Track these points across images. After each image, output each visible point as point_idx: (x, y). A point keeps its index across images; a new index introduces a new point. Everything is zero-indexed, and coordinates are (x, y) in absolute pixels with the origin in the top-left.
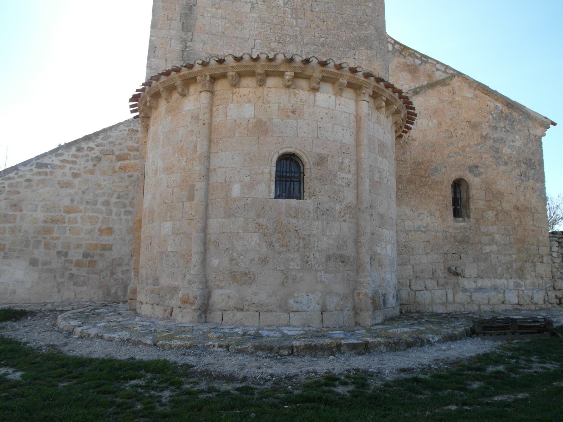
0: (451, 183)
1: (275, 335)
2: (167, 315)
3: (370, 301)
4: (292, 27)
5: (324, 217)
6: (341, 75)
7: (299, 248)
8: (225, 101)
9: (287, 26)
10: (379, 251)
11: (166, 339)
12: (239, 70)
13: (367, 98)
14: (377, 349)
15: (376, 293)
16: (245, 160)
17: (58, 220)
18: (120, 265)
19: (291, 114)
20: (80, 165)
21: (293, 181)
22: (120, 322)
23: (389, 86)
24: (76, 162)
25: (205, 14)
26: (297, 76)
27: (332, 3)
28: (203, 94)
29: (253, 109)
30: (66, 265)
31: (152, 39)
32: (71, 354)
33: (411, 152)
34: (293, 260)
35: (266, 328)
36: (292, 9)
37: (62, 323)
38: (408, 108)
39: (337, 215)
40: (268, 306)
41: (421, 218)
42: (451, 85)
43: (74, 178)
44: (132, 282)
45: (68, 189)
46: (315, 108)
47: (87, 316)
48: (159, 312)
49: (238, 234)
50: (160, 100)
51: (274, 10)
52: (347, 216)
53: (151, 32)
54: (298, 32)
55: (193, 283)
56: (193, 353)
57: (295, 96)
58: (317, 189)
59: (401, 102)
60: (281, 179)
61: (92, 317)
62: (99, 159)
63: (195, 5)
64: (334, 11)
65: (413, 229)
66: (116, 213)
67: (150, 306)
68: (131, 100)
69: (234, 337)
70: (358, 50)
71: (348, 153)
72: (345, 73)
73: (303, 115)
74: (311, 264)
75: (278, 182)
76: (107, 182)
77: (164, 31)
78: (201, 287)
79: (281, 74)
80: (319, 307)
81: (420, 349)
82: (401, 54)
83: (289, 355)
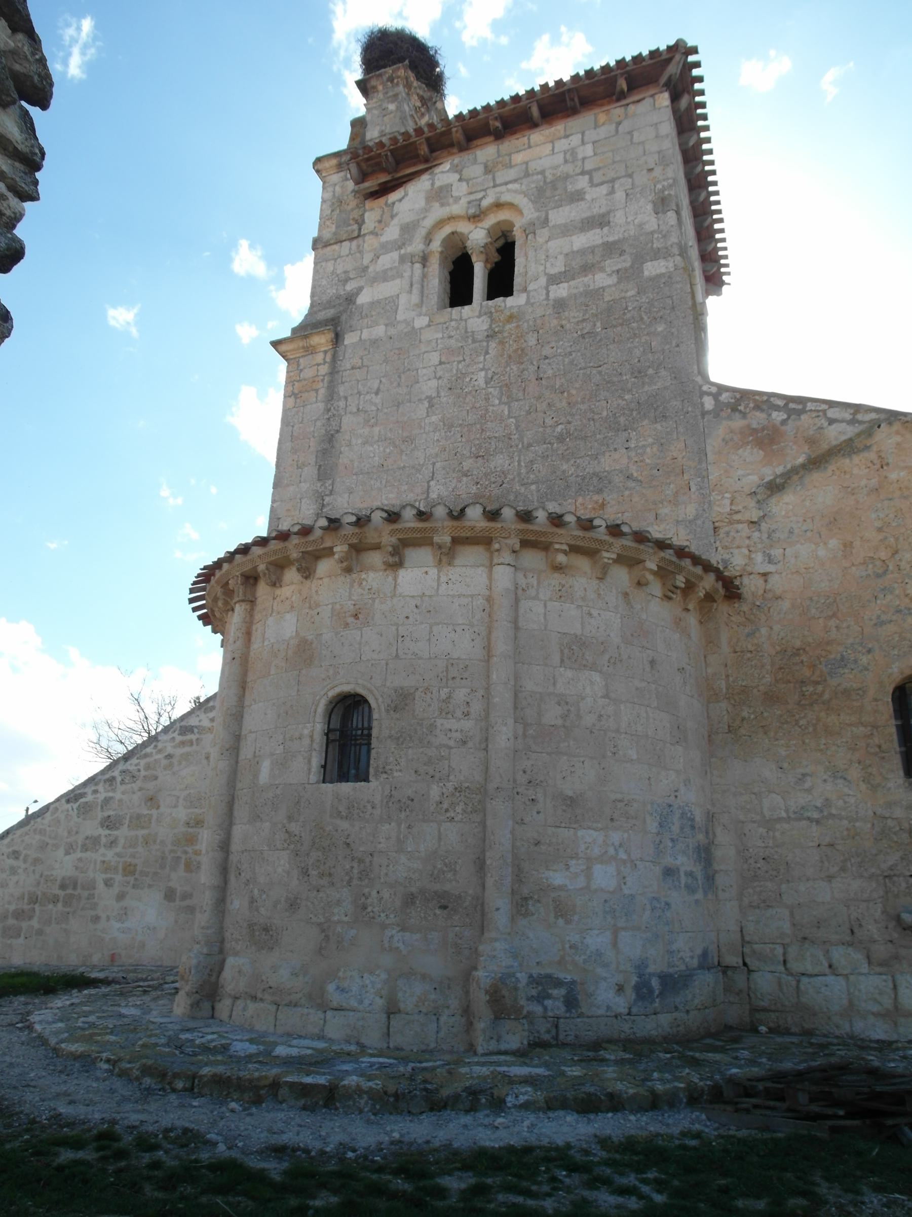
0: (890, 689)
5: (403, 813)
6: (434, 530)
9: (492, 421)
14: (351, 1103)
16: (279, 716)
19: (350, 620)
25: (354, 442)
27: (579, 351)
33: (771, 628)
34: (339, 903)
39: (432, 808)
40: (290, 994)
41: (807, 785)
42: (875, 448)
51: (469, 398)
52: (459, 809)
54: (513, 427)
58: (391, 759)
63: (338, 431)
64: (583, 365)
65: (784, 814)
70: (634, 430)
71: (464, 676)
72: (439, 524)
73: (373, 619)
77: (291, 488)
80: (380, 1002)
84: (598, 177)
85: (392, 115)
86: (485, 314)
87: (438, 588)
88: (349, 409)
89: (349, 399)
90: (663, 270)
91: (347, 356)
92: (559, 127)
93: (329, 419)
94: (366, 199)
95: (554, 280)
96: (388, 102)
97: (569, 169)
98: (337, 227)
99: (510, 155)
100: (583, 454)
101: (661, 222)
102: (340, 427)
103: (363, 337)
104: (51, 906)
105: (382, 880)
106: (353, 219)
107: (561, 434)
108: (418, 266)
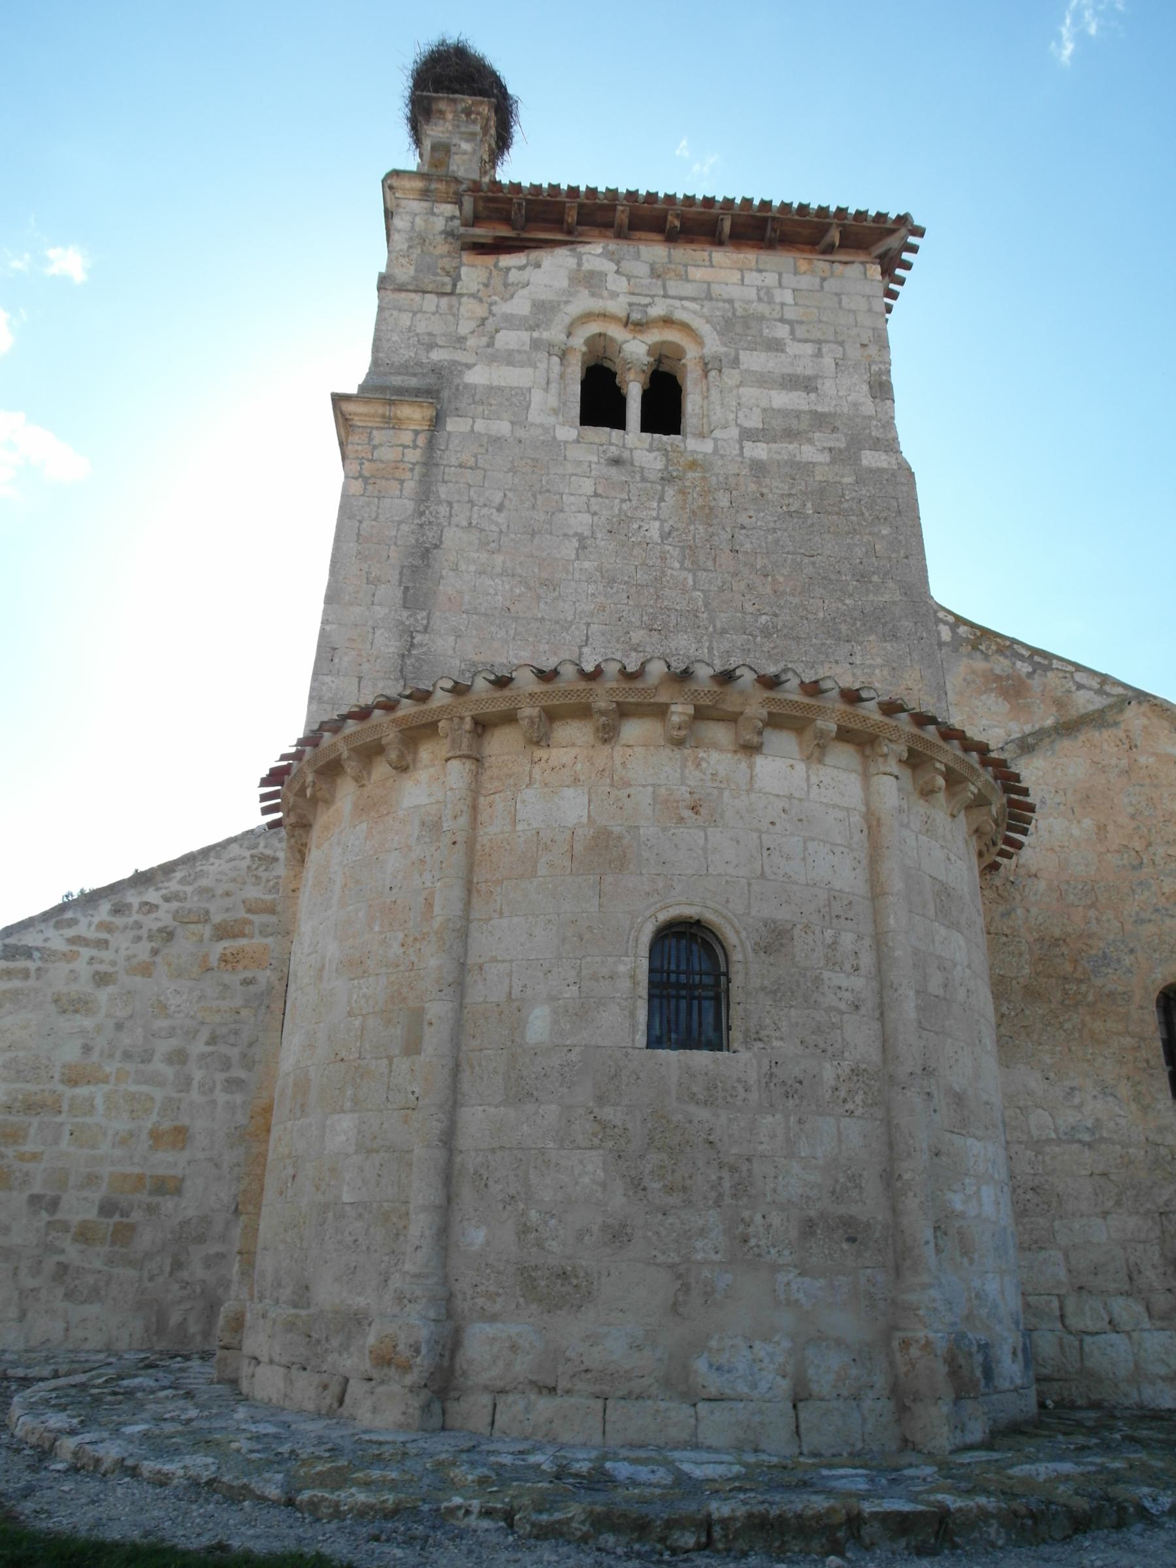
0: (1155, 996)
1: (654, 1479)
2: (328, 1401)
3: (942, 1369)
4: (684, 591)
5: (791, 1102)
6: (821, 711)
7: (721, 1195)
8: (511, 781)
10: (959, 1207)
11: (323, 1485)
12: (550, 703)
13: (893, 766)
14: (976, 1535)
15: (958, 1339)
16: (564, 940)
17: (43, 1106)
18: (201, 1239)
19: (687, 813)
20: (117, 952)
21: (700, 998)
22: (190, 1420)
23: (949, 734)
24: (106, 942)
25: (463, 567)
26: (701, 714)
28: (454, 764)
29: (587, 801)
30: (50, 1238)
31: (328, 628)
32: (43, 1524)
33: (1028, 911)
34: (702, 1232)
35: (624, 1453)
36: (682, 547)
37: (22, 1420)
38: (1007, 789)
39: (828, 1096)
40: (630, 1380)
41: (1077, 1101)
42: (1123, 726)
43: (99, 986)
44: (232, 1294)
45: (78, 1016)
46: (753, 796)
47: (97, 1400)
48: (305, 1391)
49: (542, 1151)
50: (339, 781)
52: (859, 1098)
53: (325, 612)
54: (700, 603)
55: (410, 1301)
56: (404, 1534)
57: (699, 765)
59: (987, 775)
60: (665, 992)
61: (112, 1403)
62: (168, 935)
63: (436, 547)
64: (791, 549)
65: (1053, 1136)
66: (201, 1085)
67: (282, 1370)
68: (265, 782)
69: (527, 1481)
71: (849, 916)
72: (829, 705)
73: (722, 817)
74: (758, 1246)
75: (656, 1002)
76: (184, 997)
77: (357, 610)
78: (432, 1314)
79: (661, 712)
80: (784, 1385)
81: (1114, 1537)
82: (975, 648)
83: (700, 1548)
84: (800, 332)
85: (466, 157)
86: (658, 450)
87: (808, 791)
88: (454, 520)
89: (456, 506)
90: (885, 465)
91: (451, 447)
92: (750, 256)
93: (421, 526)
94: (462, 249)
95: (748, 435)
96: (461, 139)
97: (763, 308)
98: (416, 271)
99: (686, 266)
100: (796, 658)
101: (879, 410)
102: (441, 542)
103: (476, 428)
105: (769, 1199)
106: (443, 269)
107: (766, 626)
108: (555, 360)
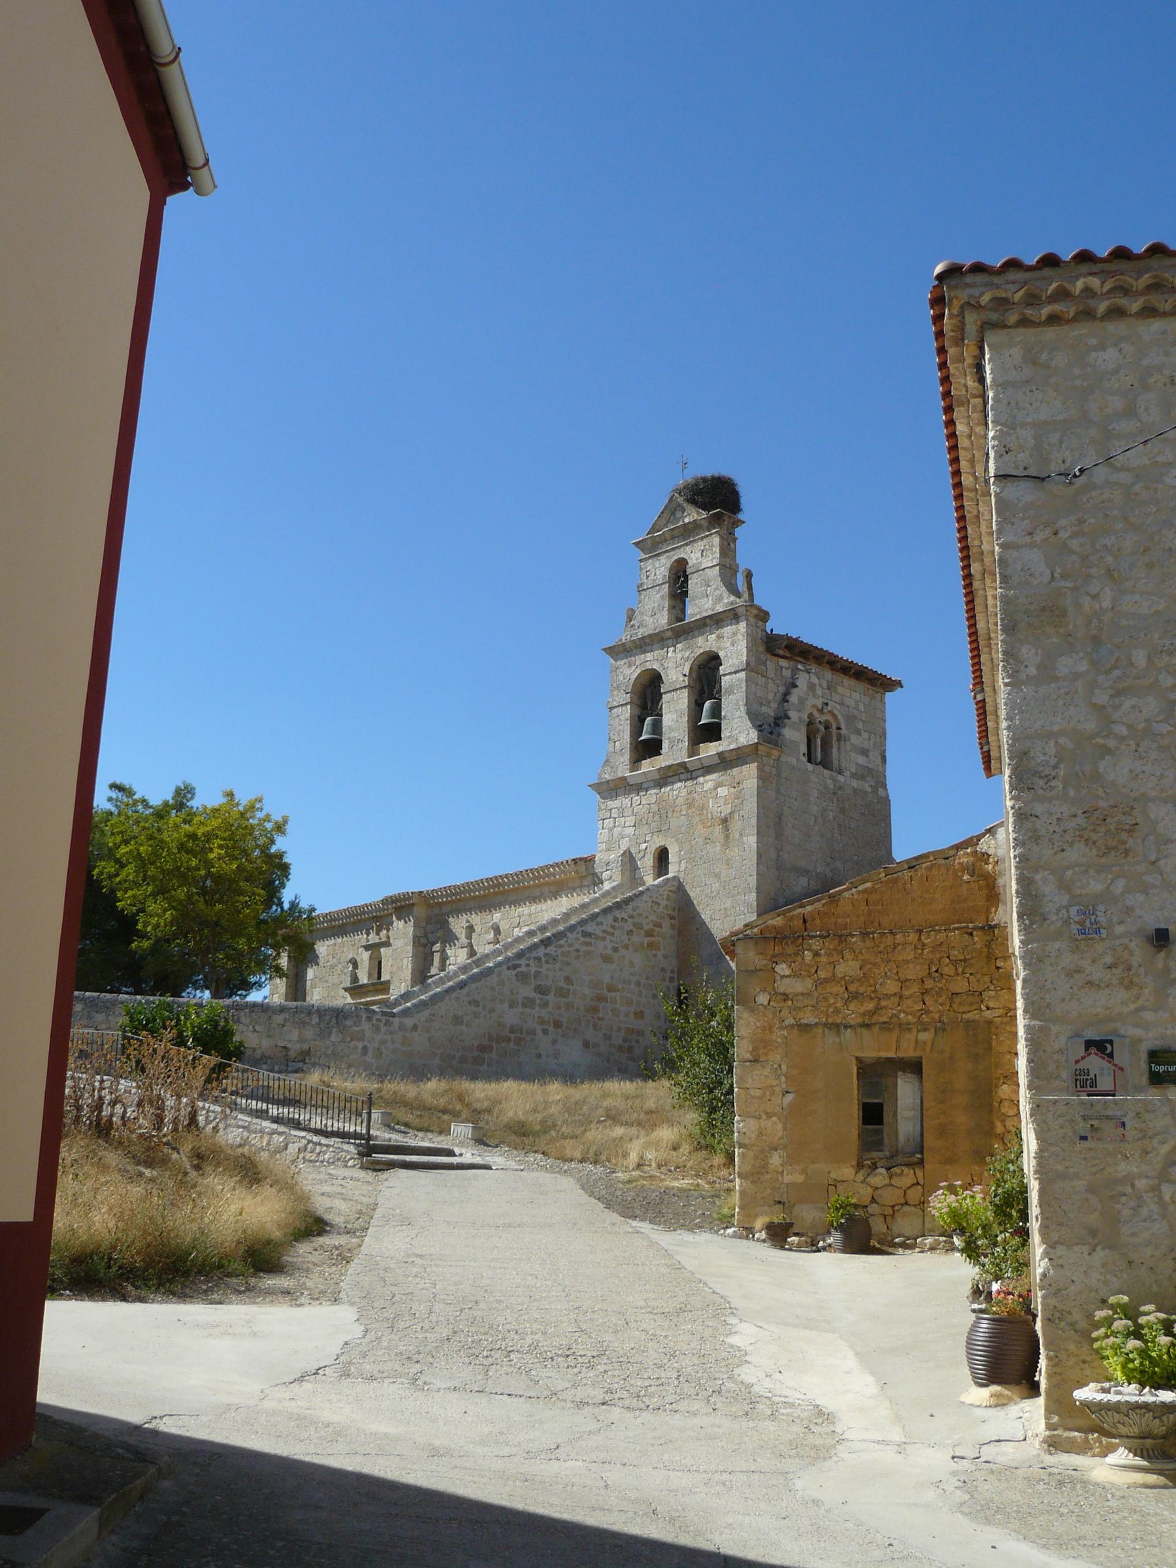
104: (504, 1045)
